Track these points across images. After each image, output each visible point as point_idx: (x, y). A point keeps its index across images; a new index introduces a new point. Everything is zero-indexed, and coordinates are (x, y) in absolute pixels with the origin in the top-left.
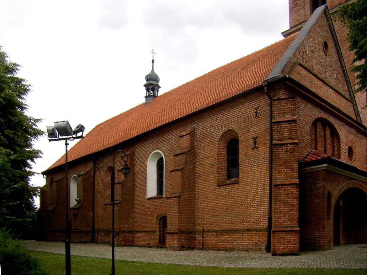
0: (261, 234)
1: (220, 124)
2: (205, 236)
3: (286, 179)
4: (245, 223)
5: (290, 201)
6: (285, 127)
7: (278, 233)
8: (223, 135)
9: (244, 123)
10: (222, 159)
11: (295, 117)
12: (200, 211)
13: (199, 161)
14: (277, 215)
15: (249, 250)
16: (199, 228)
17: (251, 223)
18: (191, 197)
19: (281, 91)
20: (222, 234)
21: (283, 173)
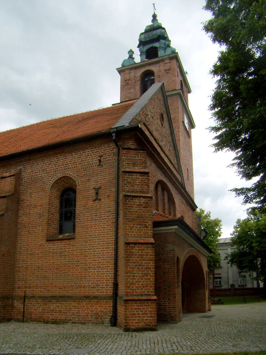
0: (104, 303)
1: (54, 169)
2: (27, 303)
3: (138, 237)
4: (82, 289)
5: (145, 263)
6: (136, 178)
7: (131, 302)
8: (56, 182)
9: (83, 171)
10: (54, 210)
11: (146, 170)
12: (22, 270)
13: (24, 209)
14: (129, 280)
15: (88, 323)
16: (20, 292)
17: (91, 289)
18: (11, 252)
19: (131, 142)
20: (52, 301)
21: (135, 230)
